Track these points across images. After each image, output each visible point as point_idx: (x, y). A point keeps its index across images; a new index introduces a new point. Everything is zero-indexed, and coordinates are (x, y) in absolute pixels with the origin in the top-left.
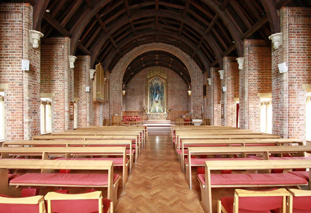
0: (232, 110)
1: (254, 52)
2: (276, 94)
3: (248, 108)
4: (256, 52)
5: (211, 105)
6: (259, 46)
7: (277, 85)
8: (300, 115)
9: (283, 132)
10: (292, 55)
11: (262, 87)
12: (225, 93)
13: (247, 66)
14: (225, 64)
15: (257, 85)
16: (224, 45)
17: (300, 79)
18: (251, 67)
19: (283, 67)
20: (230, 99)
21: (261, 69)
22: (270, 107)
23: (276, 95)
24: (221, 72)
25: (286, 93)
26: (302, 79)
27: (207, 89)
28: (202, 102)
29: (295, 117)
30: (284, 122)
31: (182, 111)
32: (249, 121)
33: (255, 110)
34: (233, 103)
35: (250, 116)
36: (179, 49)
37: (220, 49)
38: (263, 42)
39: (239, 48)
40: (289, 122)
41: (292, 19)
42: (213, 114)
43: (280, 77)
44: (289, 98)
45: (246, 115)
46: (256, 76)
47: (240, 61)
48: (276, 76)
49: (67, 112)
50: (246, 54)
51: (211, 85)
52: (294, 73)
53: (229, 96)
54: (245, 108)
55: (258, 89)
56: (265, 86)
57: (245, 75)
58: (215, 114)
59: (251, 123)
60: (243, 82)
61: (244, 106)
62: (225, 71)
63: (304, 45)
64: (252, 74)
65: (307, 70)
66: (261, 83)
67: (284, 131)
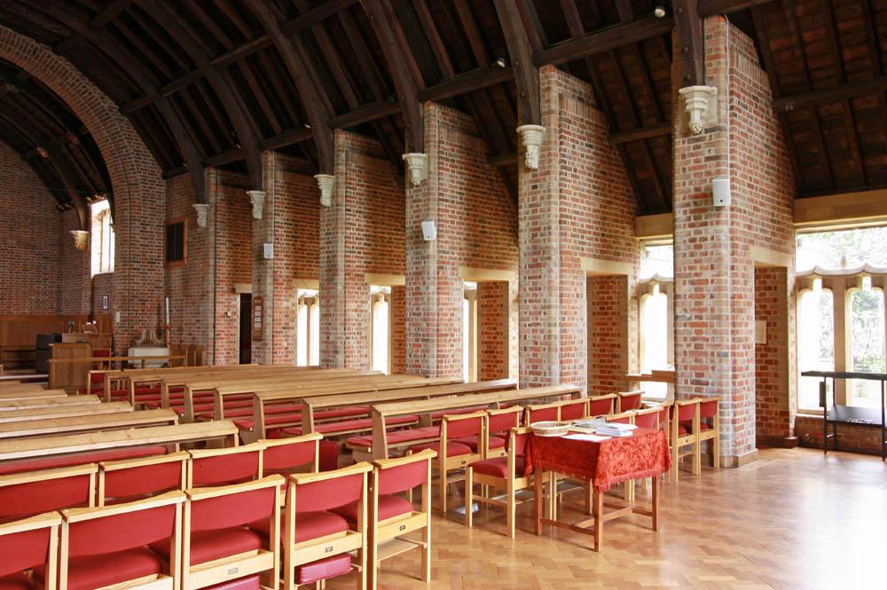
0: (286, 316)
1: (360, 167)
2: (415, 283)
3: (345, 311)
4: (363, 168)
5: (204, 295)
6: (368, 153)
7: (416, 263)
8: (455, 330)
9: (428, 367)
10: (444, 205)
11: (373, 258)
12: (268, 262)
13: (342, 201)
14: (269, 172)
15: (364, 253)
16: (274, 122)
17: (456, 256)
18: (351, 206)
19: (430, 230)
20: (281, 280)
21: (373, 214)
22: (316, 311)
23: (414, 287)
24: (256, 196)
25: (434, 284)
26: (458, 256)
27: (186, 239)
28: (161, 284)
29: (447, 335)
30: (430, 344)
31: (31, 316)
32: (347, 345)
33: (360, 319)
34: (290, 296)
35: (350, 334)
36: (69, 67)
37: (255, 126)
38: (376, 146)
39: (322, 144)
40: (438, 346)
41: (444, 131)
42: (214, 327)
43: (423, 248)
44: (438, 293)
45: (340, 330)
46: (362, 230)
47: (325, 182)
48: (415, 243)
49: (553, 304)
50: (342, 168)
51: (207, 229)
52: (446, 242)
53: (279, 273)
54: (336, 311)
55: (365, 262)
56: (381, 262)
57: (337, 224)
58: (219, 328)
59: (352, 352)
60: (332, 242)
61: (335, 306)
62: (269, 197)
63: (461, 188)
64: (355, 225)
65: (465, 239)
66: (373, 249)
67: (430, 364)
